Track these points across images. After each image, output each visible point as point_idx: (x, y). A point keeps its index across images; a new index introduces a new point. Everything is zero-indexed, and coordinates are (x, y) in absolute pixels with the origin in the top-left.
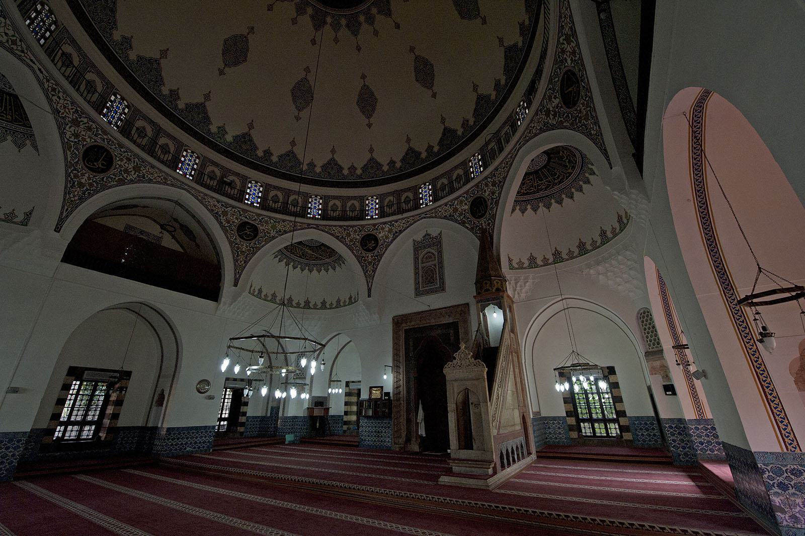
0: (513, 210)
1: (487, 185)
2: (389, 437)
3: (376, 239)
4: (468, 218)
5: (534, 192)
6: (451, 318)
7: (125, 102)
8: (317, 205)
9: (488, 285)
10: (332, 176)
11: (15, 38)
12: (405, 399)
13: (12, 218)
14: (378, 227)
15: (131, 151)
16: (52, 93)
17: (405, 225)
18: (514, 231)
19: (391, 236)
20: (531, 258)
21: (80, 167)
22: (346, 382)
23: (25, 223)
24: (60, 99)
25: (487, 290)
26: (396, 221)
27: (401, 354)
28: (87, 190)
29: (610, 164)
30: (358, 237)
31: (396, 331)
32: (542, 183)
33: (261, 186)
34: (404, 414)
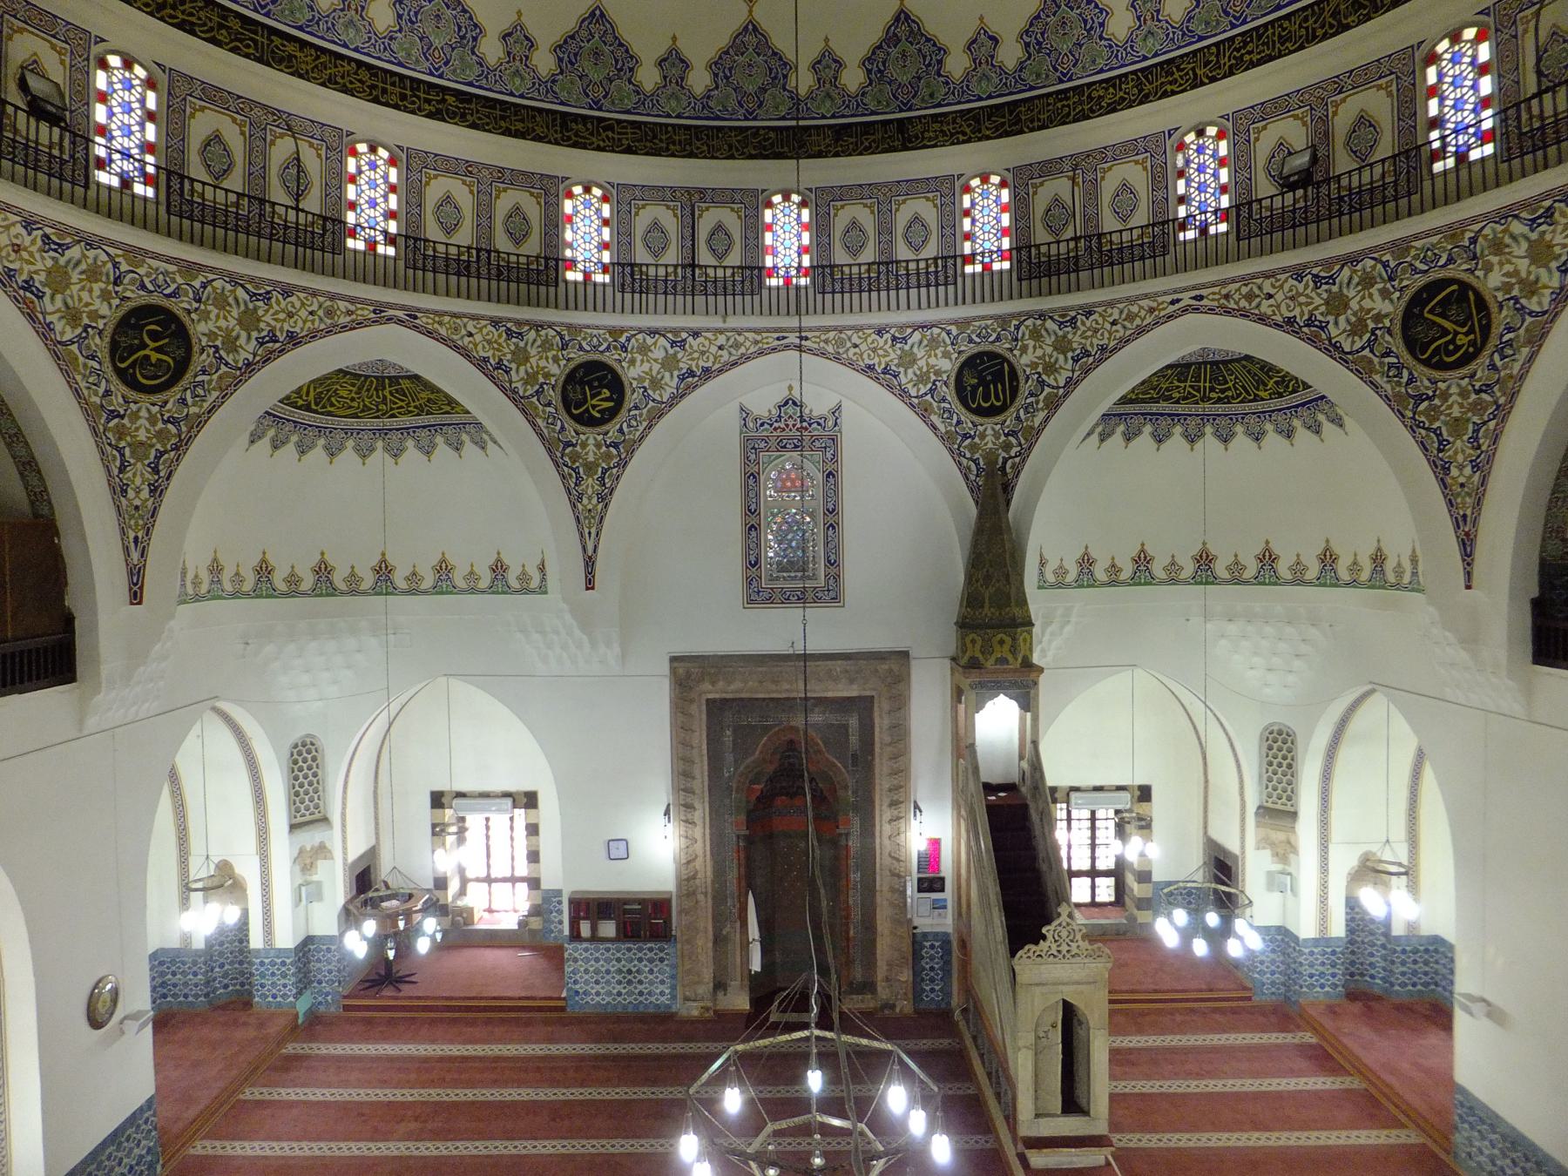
1: (1036, 335)
2: (662, 982)
3: (617, 386)
9: (1006, 647)
11: (1254, 304)
14: (628, 340)
15: (1029, 315)
17: (724, 353)
18: (1080, 491)
19: (671, 383)
22: (433, 793)
25: (1003, 661)
26: (696, 334)
27: (697, 772)
28: (604, 472)
29: (1469, 575)
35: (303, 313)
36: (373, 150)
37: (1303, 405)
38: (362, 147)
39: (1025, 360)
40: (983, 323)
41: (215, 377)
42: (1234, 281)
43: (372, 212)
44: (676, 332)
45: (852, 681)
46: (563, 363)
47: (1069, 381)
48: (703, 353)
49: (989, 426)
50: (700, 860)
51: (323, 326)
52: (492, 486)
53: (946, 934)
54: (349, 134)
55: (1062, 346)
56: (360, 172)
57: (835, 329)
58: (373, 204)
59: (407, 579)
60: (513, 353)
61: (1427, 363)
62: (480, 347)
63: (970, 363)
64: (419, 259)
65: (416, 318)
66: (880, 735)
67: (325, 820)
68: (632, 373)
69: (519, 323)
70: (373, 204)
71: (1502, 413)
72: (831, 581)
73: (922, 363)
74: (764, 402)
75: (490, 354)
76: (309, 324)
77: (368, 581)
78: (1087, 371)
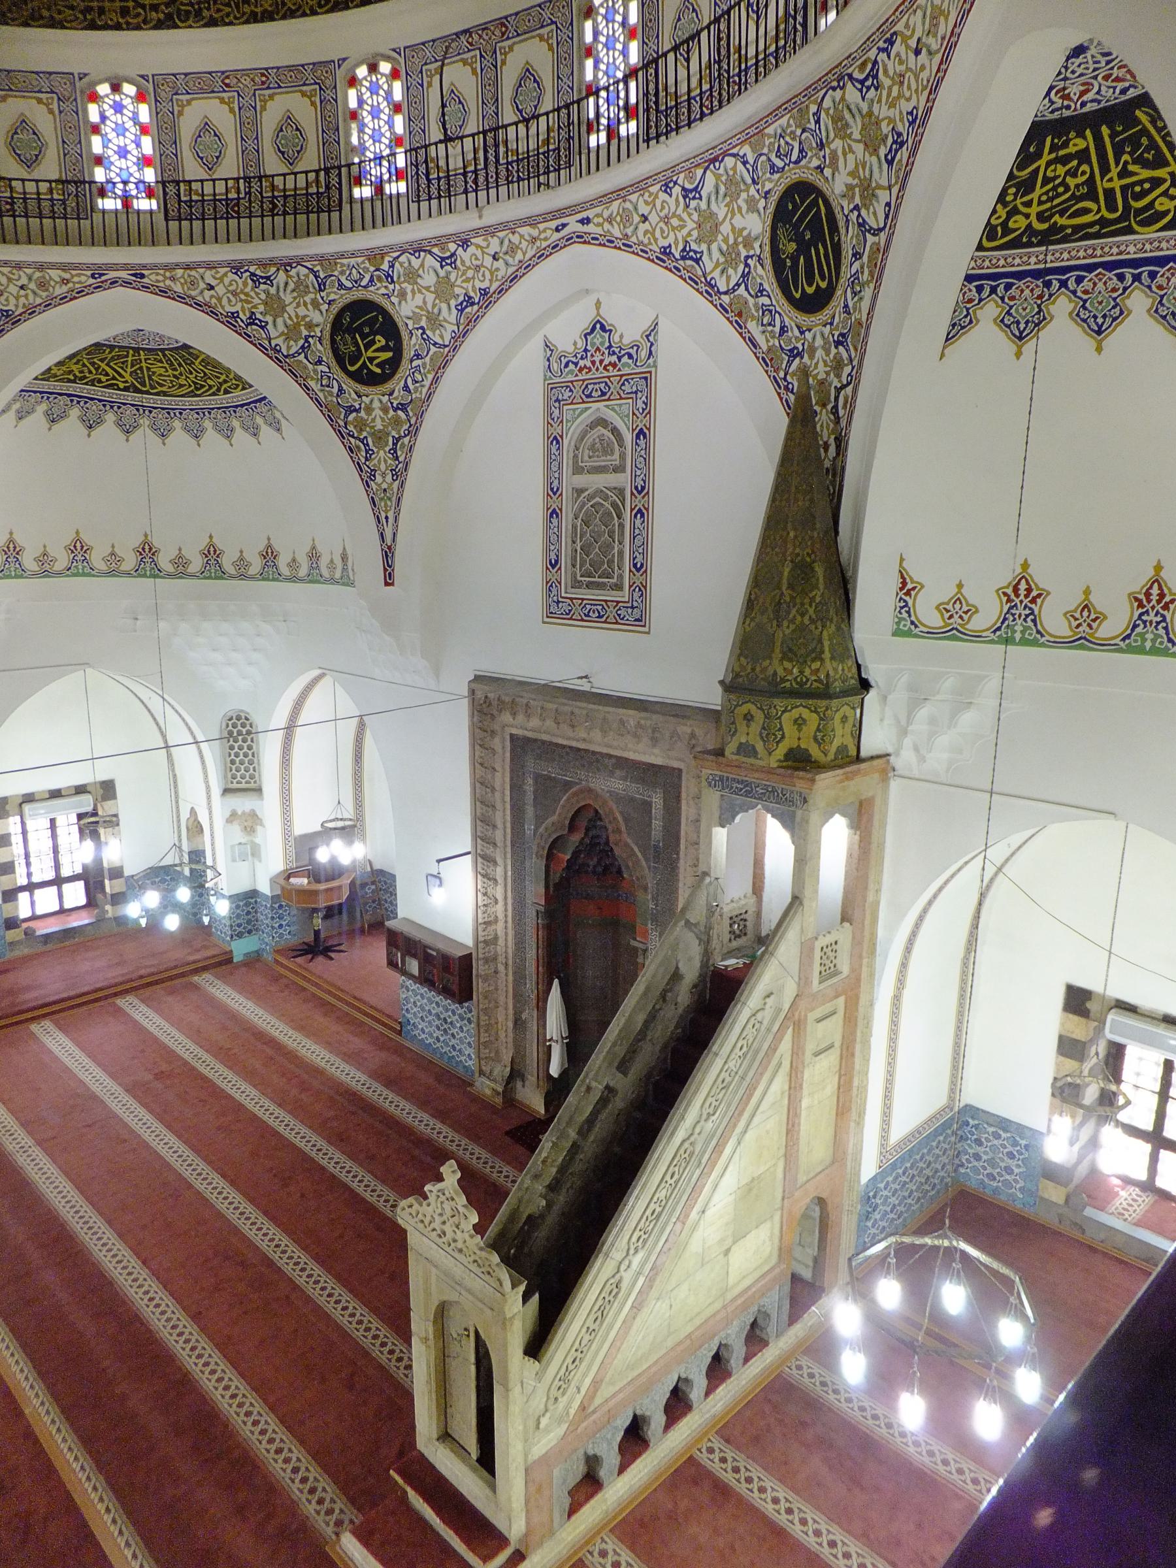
0: (958, 327)
3: (390, 329)
4: (761, 291)
5: (1103, 229)
6: (656, 751)
9: (755, 727)
12: (510, 962)
13: (961, 617)
17: (500, 264)
20: (1016, 590)
28: (396, 441)
31: (481, 734)
32: (1156, 182)
34: (506, 1000)
35: (13, 289)
36: (116, 88)
38: (103, 89)
41: (428, 359)
43: (123, 163)
44: (441, 241)
45: (654, 741)
46: (325, 307)
48: (477, 268)
50: (500, 927)
51: (38, 301)
52: (286, 466)
54: (82, 76)
56: (103, 118)
58: (123, 153)
60: (266, 303)
62: (225, 301)
64: (186, 207)
65: (143, 276)
67: (259, 790)
68: (405, 310)
69: (263, 264)
70: (123, 153)
72: (636, 595)
73: (725, 228)
74: (567, 333)
75: (238, 308)
76: (22, 300)
77: (256, 566)
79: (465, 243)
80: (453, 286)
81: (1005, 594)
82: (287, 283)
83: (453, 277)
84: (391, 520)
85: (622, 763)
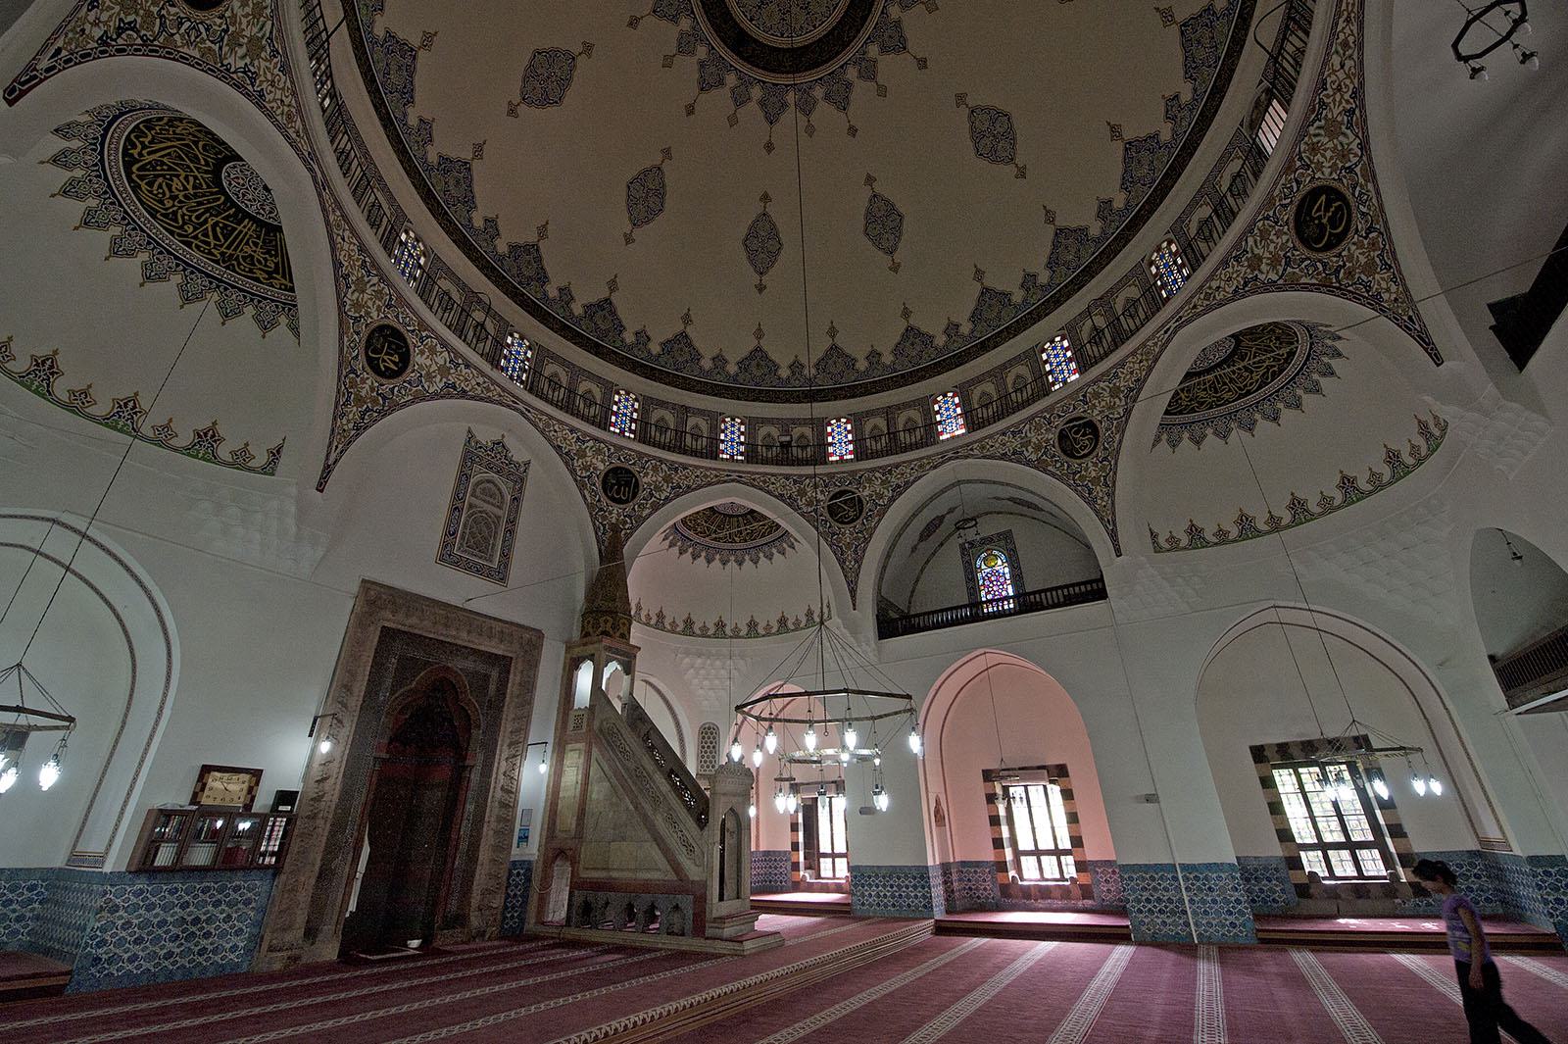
0: (1157, 440)
1: (655, 469)
3: (405, 360)
7: (631, 395)
8: (735, 436)
10: (754, 382)
13: (244, 460)
14: (427, 337)
15: (654, 458)
16: (1339, 49)
19: (438, 385)
21: (1335, 259)
23: (269, 469)
24: (1342, 67)
28: (368, 410)
29: (854, 605)
30: (374, 314)
33: (636, 400)
37: (766, 544)
39: (645, 480)
40: (1373, 194)
41: (208, 44)
42: (757, 474)
44: (458, 354)
47: (667, 498)
49: (616, 509)
53: (530, 862)
55: (667, 479)
57: (547, 415)
59: (72, 392)
61: (837, 521)
62: (343, 253)
63: (615, 471)
66: (512, 688)
71: (867, 541)
73: (588, 459)
76: (274, 104)
78: (678, 496)
79: (467, 366)
80: (449, 374)
81: (198, 434)
82: (374, 285)
83: (452, 371)
84: (338, 450)
85: (475, 651)
